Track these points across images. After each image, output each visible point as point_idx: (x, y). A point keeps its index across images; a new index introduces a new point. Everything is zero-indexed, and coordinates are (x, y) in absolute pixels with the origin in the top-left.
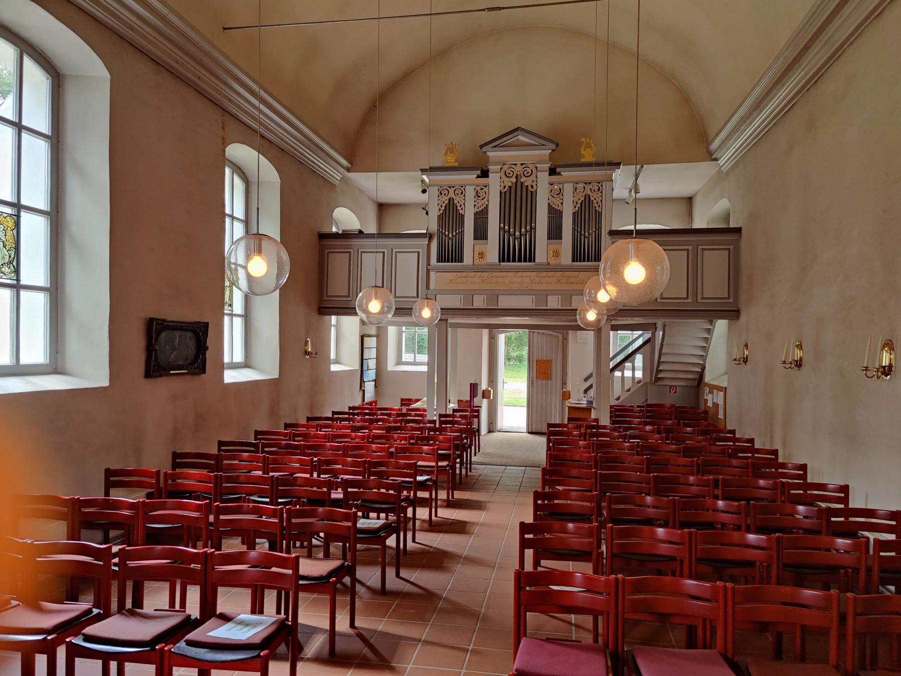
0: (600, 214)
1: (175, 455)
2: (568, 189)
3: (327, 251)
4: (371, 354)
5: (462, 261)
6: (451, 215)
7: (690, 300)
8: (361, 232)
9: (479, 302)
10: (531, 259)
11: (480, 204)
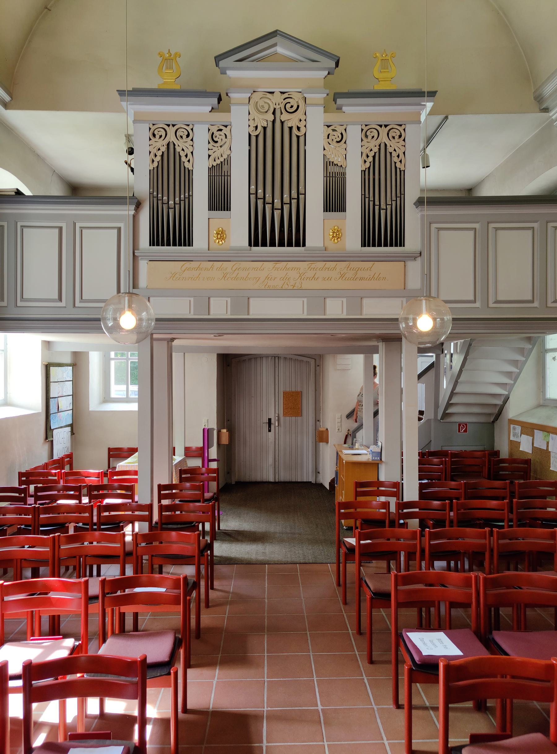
0: (402, 173)
2: (354, 134)
4: (63, 389)
5: (402, 244)
6: (170, 171)
7: (536, 304)
8: (18, 193)
9: (220, 308)
10: (300, 242)
11: (218, 154)
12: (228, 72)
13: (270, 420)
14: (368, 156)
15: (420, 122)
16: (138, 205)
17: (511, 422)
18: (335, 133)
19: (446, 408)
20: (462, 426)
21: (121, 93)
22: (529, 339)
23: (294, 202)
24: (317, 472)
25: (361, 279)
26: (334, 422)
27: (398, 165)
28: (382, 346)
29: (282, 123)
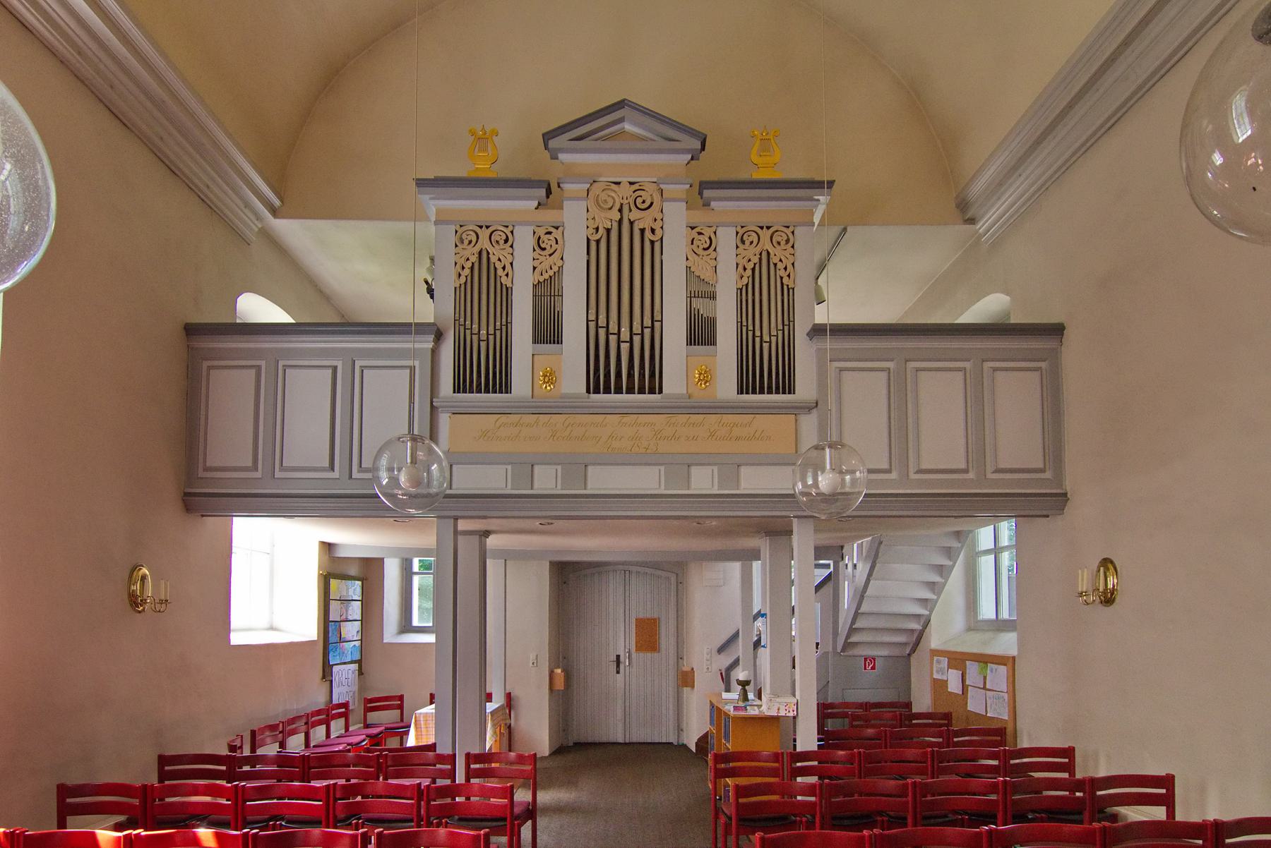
1: (163, 760)
2: (726, 239)
3: (205, 364)
5: (791, 391)
6: (482, 286)
9: (546, 480)
10: (655, 386)
11: (546, 265)
12: (561, 156)
13: (618, 657)
14: (745, 269)
15: (813, 224)
16: (439, 336)
17: (935, 653)
18: (701, 237)
19: (848, 637)
20: (870, 661)
21: (422, 183)
22: (958, 534)
23: (647, 331)
24: (680, 730)
25: (738, 439)
26: (703, 660)
27: (785, 280)
28: (763, 544)
29: (631, 223)
